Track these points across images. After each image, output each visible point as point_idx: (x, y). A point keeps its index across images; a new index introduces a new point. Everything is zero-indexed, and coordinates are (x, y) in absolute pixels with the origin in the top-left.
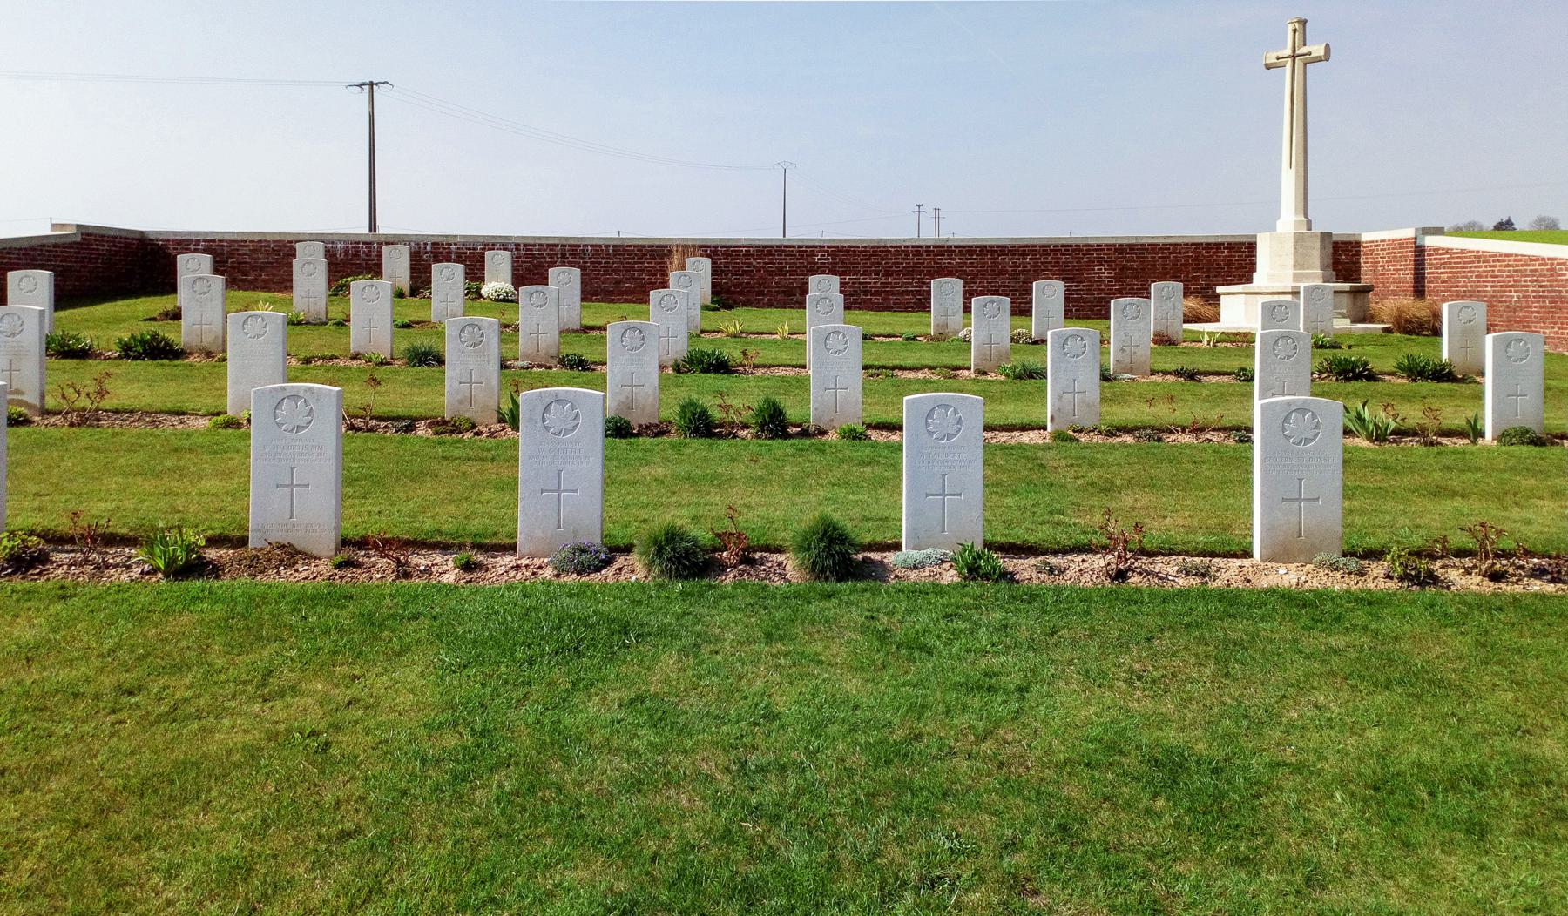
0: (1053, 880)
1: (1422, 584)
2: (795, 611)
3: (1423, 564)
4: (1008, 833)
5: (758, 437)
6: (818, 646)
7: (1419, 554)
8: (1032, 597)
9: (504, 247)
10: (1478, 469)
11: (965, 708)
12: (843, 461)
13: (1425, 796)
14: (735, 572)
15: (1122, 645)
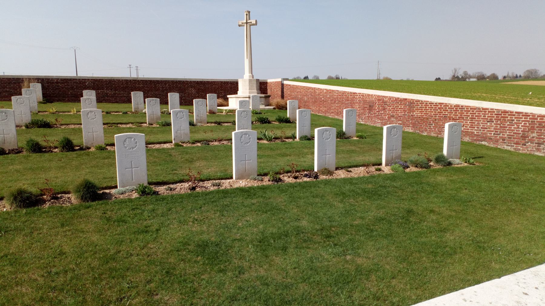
0: (163, 290)
1: (277, 182)
2: (74, 214)
3: (278, 176)
4: (149, 278)
5: (62, 151)
6: (83, 226)
7: (277, 173)
8: (164, 199)
10: (294, 148)
11: (137, 239)
12: (97, 158)
13: (272, 242)
14: (50, 203)
15: (192, 211)
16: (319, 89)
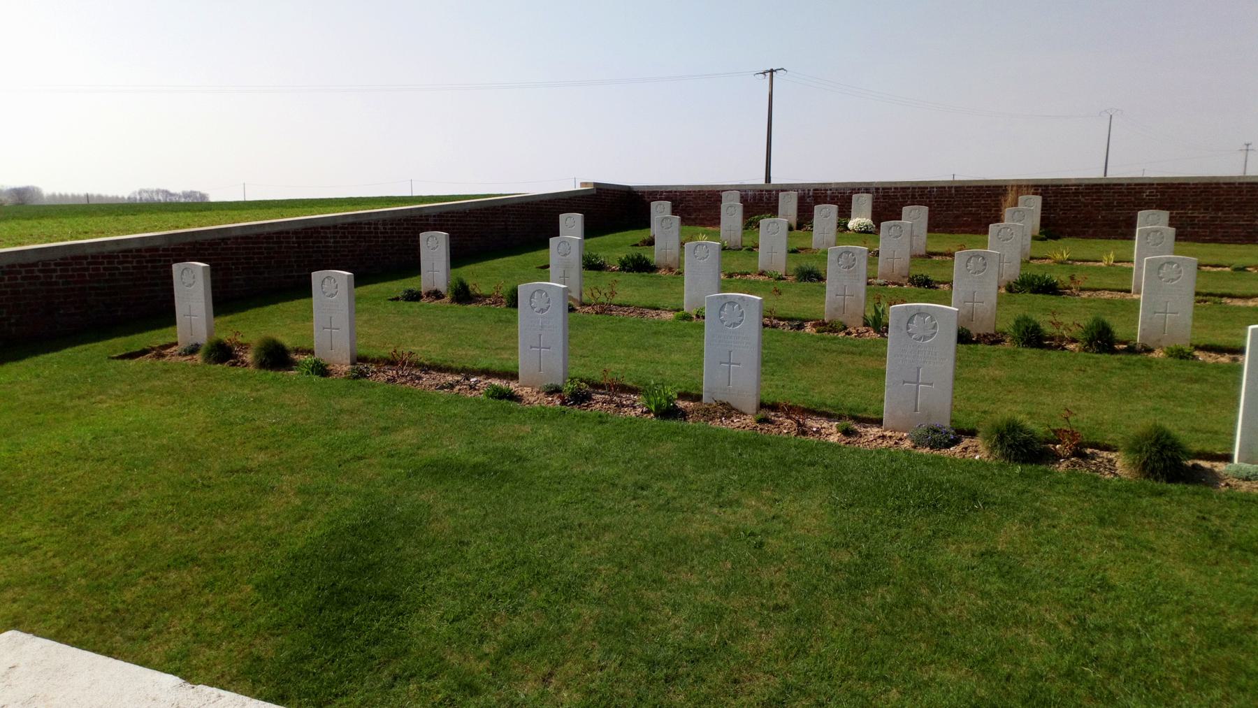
2: (1126, 501)
5: (1086, 351)
6: (1151, 535)
9: (867, 191)
12: (1169, 377)
14: (1067, 462)
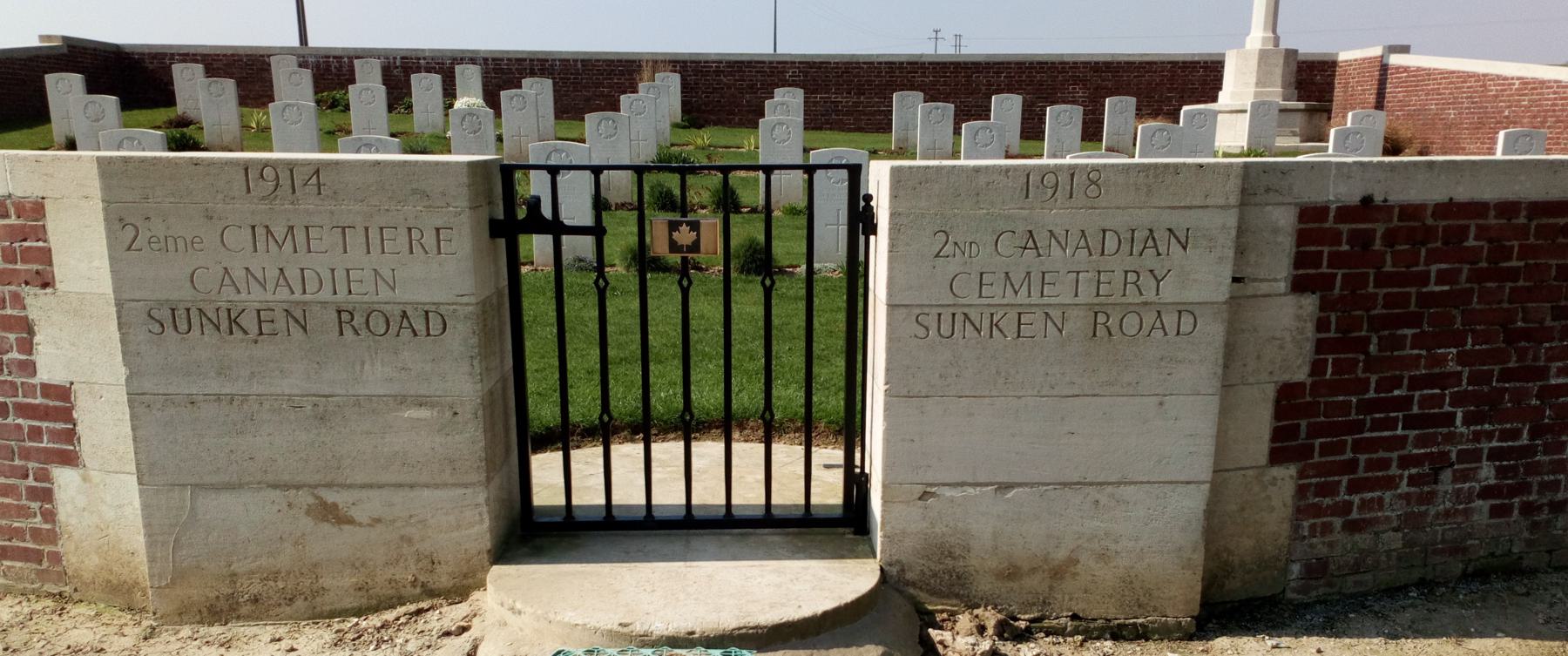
9: (473, 61)
16: (1498, 77)
